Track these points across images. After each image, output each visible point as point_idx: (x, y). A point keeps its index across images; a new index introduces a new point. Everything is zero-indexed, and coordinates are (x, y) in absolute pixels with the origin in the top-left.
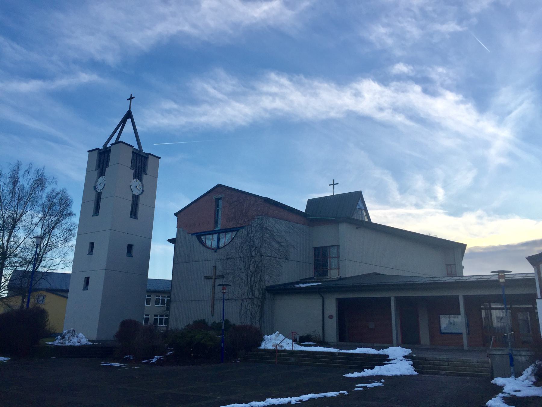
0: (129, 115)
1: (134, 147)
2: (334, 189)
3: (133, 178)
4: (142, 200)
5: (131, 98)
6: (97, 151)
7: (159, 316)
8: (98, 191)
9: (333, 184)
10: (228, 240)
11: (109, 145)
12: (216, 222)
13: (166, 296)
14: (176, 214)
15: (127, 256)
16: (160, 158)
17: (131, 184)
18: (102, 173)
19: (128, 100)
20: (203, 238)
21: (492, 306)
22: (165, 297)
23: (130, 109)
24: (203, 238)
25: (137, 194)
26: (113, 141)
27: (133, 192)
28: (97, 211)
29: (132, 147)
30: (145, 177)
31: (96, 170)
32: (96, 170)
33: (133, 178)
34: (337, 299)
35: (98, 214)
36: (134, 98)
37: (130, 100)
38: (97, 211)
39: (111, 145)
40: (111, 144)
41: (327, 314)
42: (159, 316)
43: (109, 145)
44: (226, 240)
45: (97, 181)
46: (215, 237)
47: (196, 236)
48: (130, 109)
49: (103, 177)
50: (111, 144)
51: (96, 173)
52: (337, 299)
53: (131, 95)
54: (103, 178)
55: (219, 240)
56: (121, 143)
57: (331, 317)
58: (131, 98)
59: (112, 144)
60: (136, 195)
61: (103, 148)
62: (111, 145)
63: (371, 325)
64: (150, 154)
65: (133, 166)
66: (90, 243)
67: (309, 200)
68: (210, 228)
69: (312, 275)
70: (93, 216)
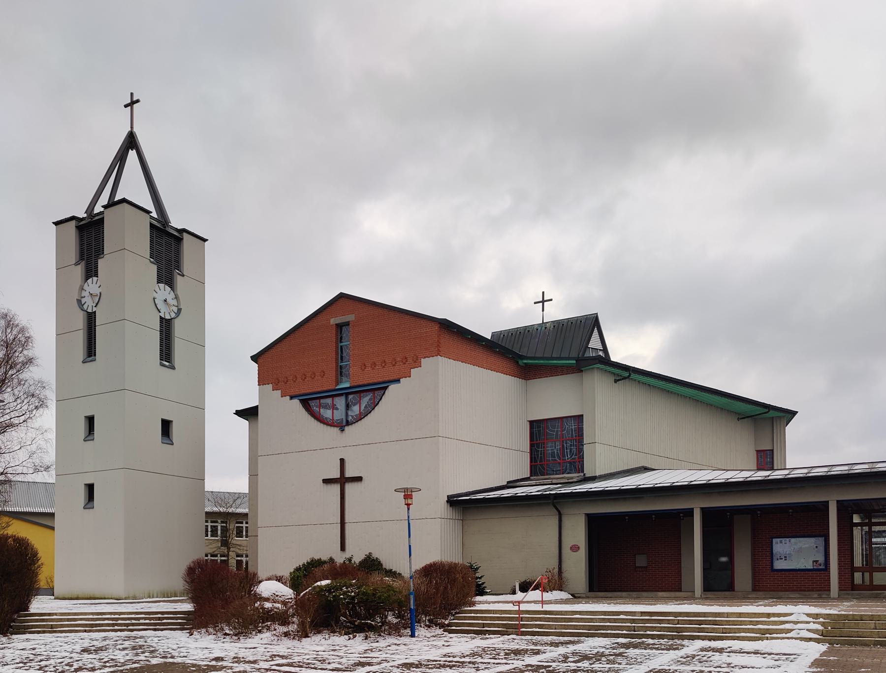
0: (131, 142)
1: (151, 212)
2: (543, 310)
3: (158, 283)
4: (179, 329)
5: (133, 103)
6: (73, 223)
7: (219, 556)
8: (88, 311)
9: (545, 303)
10: (366, 407)
11: (98, 209)
12: (341, 372)
13: (219, 521)
14: (255, 358)
15: (163, 443)
16: (207, 240)
17: (155, 295)
18: (91, 272)
19: (126, 106)
20: (312, 403)
21: (873, 520)
22: (217, 522)
23: (132, 127)
24: (312, 403)
25: (168, 317)
26: (104, 199)
27: (160, 312)
28: (91, 351)
29: (148, 212)
30: (179, 281)
31: (76, 264)
32: (76, 264)
33: (158, 283)
34: (838, 501)
35: (93, 357)
36: (138, 101)
37: (130, 107)
38: (91, 351)
39: (102, 209)
40: (102, 207)
41: (567, 543)
42: (219, 556)
43: (98, 209)
44: (363, 408)
45: (82, 289)
46: (340, 402)
47: (300, 400)
48: (132, 127)
49: (95, 279)
50: (102, 207)
51: (79, 271)
52: (838, 501)
53: (132, 94)
54: (95, 282)
55: (348, 407)
56: (125, 204)
57: (575, 548)
58: (133, 103)
59: (105, 207)
60: (166, 320)
61: (85, 215)
62: (102, 209)
63: (641, 561)
64: (184, 230)
65: (155, 255)
66: (86, 417)
68: (327, 384)
69: (527, 474)
70: (84, 362)
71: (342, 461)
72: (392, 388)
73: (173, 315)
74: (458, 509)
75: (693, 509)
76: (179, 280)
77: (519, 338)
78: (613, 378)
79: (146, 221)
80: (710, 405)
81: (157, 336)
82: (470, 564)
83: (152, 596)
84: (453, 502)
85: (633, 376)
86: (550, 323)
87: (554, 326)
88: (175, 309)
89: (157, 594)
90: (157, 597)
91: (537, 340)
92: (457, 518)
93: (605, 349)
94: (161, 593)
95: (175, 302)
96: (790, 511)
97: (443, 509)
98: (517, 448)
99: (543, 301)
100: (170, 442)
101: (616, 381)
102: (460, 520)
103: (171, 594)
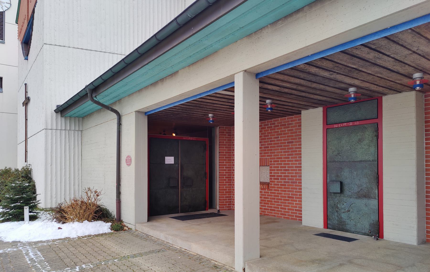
73: (5, 9)
74: (79, 121)
102: (79, 130)
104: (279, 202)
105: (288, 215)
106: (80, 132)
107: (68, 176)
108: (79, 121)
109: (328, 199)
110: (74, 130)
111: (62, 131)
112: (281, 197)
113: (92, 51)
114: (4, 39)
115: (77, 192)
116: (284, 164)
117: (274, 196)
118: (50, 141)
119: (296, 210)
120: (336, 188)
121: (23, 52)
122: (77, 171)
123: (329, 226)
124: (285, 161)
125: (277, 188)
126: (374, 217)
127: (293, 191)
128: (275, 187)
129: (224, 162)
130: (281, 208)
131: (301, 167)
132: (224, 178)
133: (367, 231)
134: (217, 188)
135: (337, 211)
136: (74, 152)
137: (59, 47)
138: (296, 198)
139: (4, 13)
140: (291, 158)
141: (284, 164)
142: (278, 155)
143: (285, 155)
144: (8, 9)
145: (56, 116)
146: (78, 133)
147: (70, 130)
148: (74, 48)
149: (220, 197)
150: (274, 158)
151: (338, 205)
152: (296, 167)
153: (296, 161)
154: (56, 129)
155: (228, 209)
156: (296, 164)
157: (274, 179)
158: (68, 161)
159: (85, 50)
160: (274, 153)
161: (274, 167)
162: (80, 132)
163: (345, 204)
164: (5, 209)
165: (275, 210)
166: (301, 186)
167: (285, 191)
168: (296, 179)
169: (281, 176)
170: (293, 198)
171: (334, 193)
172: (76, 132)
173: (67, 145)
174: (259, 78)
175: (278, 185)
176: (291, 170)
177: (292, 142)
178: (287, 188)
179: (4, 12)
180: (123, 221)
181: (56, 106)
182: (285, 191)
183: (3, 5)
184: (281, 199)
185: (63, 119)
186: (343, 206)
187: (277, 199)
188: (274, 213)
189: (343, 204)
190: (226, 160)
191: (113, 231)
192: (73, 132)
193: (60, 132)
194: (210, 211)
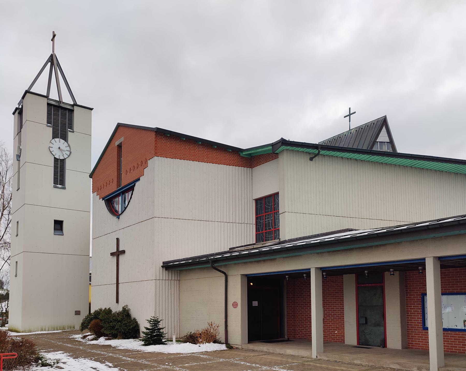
0: (52, 60)
15: (54, 234)
23: (53, 51)
30: (70, 135)
48: (53, 51)
60: (61, 160)
67: (282, 138)
69: (254, 242)
71: (118, 239)
72: (137, 184)
73: (66, 156)
74: (177, 273)
75: (424, 259)
76: (70, 135)
77: (334, 142)
78: (308, 157)
79: (45, 101)
80: (449, 173)
81: (52, 169)
82: (154, 317)
83: (44, 330)
84: (167, 266)
85: (322, 152)
86: (354, 129)
87: (356, 131)
88: (68, 153)
89: (49, 328)
90: (45, 330)
91: (344, 143)
92: (176, 279)
93: (391, 142)
94: (52, 327)
95: (68, 149)
96: (420, 268)
97: (158, 274)
98: (241, 222)
99: (350, 115)
100: (62, 234)
101: (311, 159)
102: (177, 280)
103: (60, 327)
104: (330, 331)
105: (336, 339)
106: (178, 281)
107: (170, 315)
108: (177, 273)
109: (359, 328)
110: (174, 280)
111: (166, 281)
112: (332, 328)
113: (186, 220)
114: (64, 185)
115: (176, 327)
116: (333, 306)
117: (327, 327)
118: (158, 289)
119: (341, 336)
120: (363, 321)
121: (107, 209)
122: (176, 310)
123: (360, 343)
124: (334, 304)
125: (329, 322)
126: (383, 337)
127: (339, 324)
128: (327, 322)
129: (290, 305)
130: (332, 335)
131: (343, 308)
132: (290, 315)
133: (379, 344)
134: (285, 323)
135: (364, 334)
136: (174, 296)
137: (165, 218)
138: (341, 328)
139: (64, 160)
140: (338, 302)
141: (333, 306)
142: (329, 301)
143: (334, 300)
144: (69, 156)
145: (162, 270)
146: (177, 282)
147: (171, 280)
148: (174, 218)
149: (288, 329)
150: (327, 303)
151: (365, 331)
152: (341, 308)
153: (340, 304)
154: (162, 280)
155: (294, 338)
156: (341, 306)
157: (327, 316)
158: (170, 303)
159: (181, 220)
160: (327, 299)
161: (327, 308)
162: (178, 281)
163: (368, 330)
164: (87, 344)
165: (327, 337)
166: (344, 320)
167: (334, 324)
168: (341, 316)
169: (336, 314)
170: (339, 328)
171: (362, 324)
172: (175, 281)
173: (170, 291)
174: (322, 270)
175: (330, 320)
176: (338, 310)
177: (338, 292)
178: (337, 304)
179: (65, 159)
180: (230, 343)
181: (162, 262)
182: (334, 324)
183: (64, 153)
184: (332, 329)
185: (167, 272)
186: (367, 331)
187: (329, 329)
188: (327, 339)
189: (367, 330)
190: (291, 303)
191: (228, 349)
192: (173, 281)
193: (165, 281)
194: (280, 339)
